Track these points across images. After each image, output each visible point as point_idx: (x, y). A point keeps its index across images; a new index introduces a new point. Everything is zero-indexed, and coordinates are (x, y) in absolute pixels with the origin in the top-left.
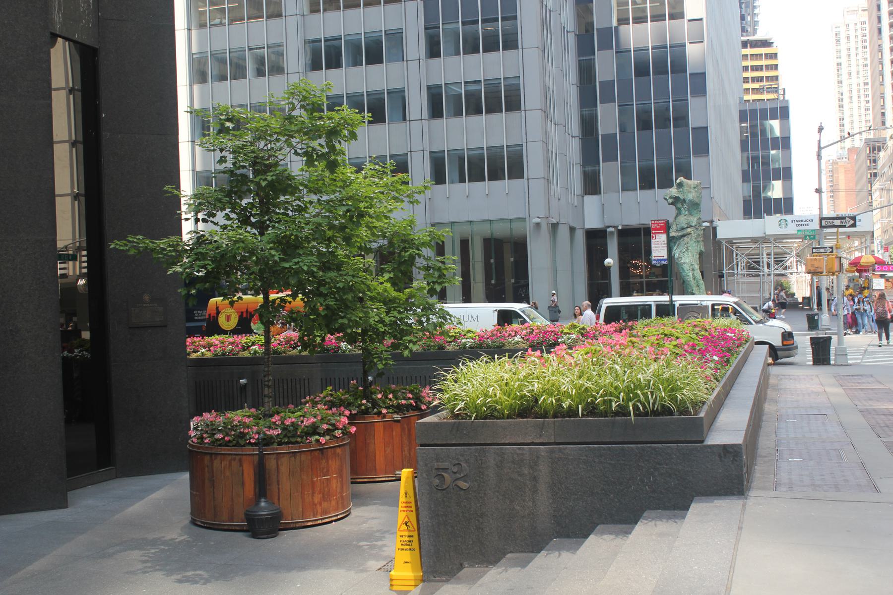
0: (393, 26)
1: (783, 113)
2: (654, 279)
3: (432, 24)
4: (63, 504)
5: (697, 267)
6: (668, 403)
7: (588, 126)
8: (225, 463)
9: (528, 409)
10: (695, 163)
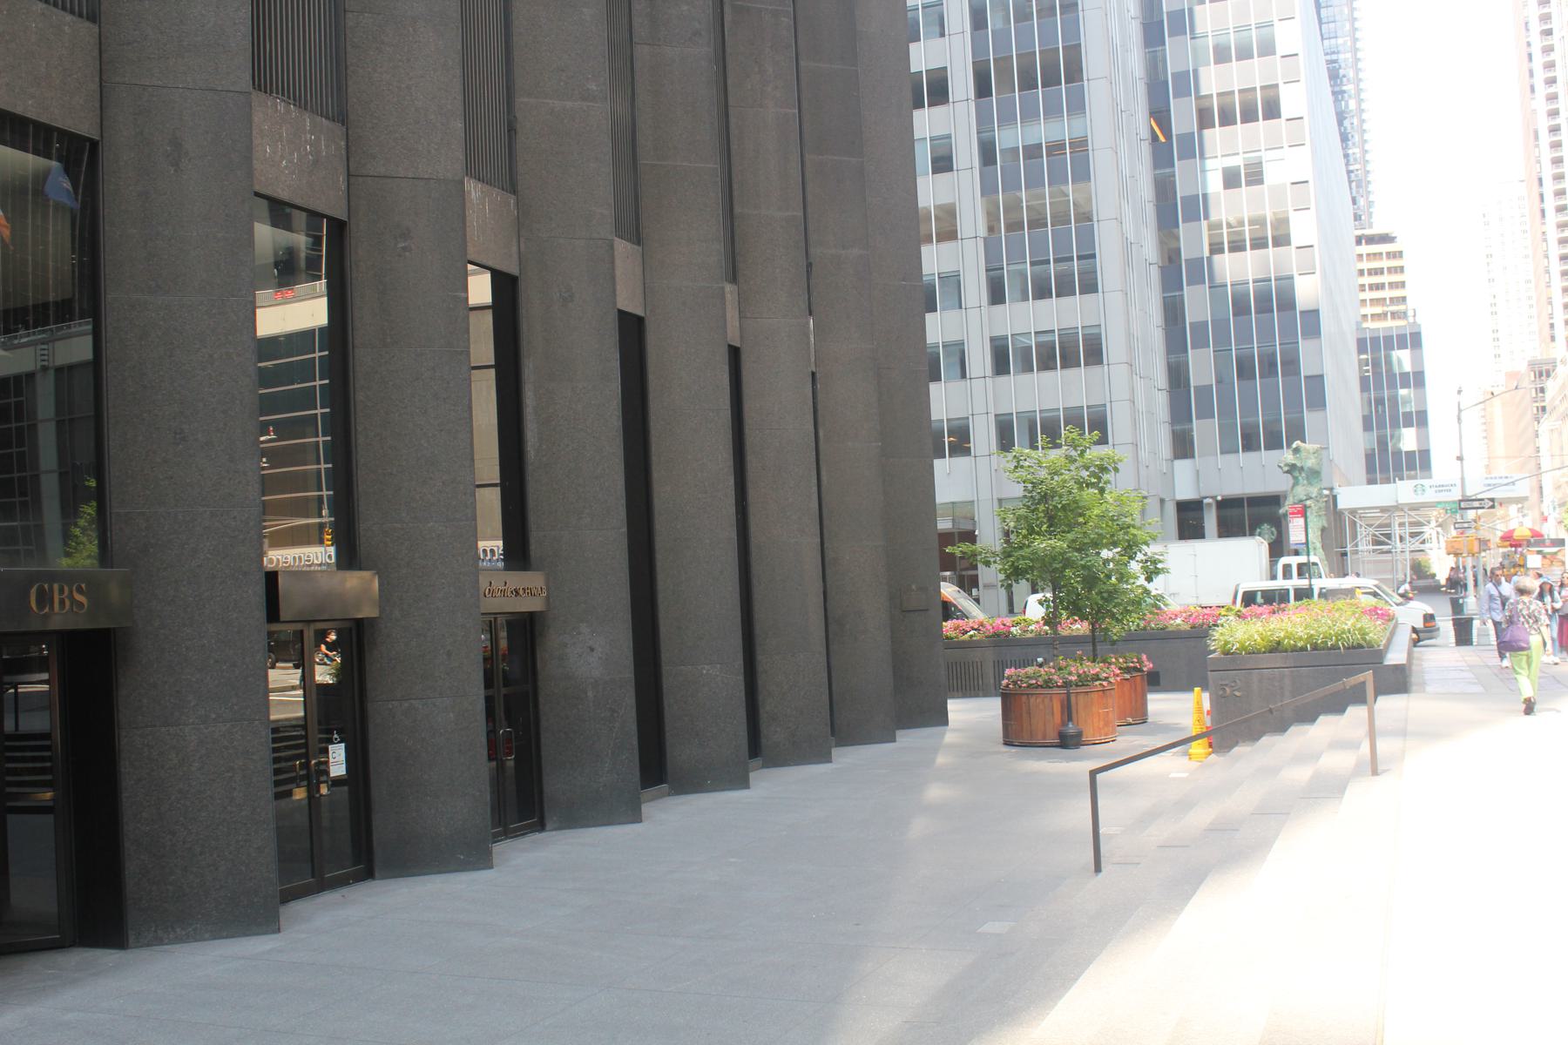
1: (1414, 340)
3: (996, 265)
4: (744, 783)
7: (1177, 377)
9: (1276, 648)
10: (1309, 418)
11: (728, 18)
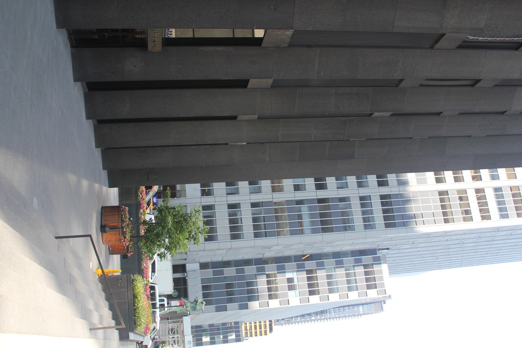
0: (263, 189)
1: (238, 339)
3: (264, 205)
4: (88, 118)
7: (227, 264)
9: (135, 297)
11: (343, 118)
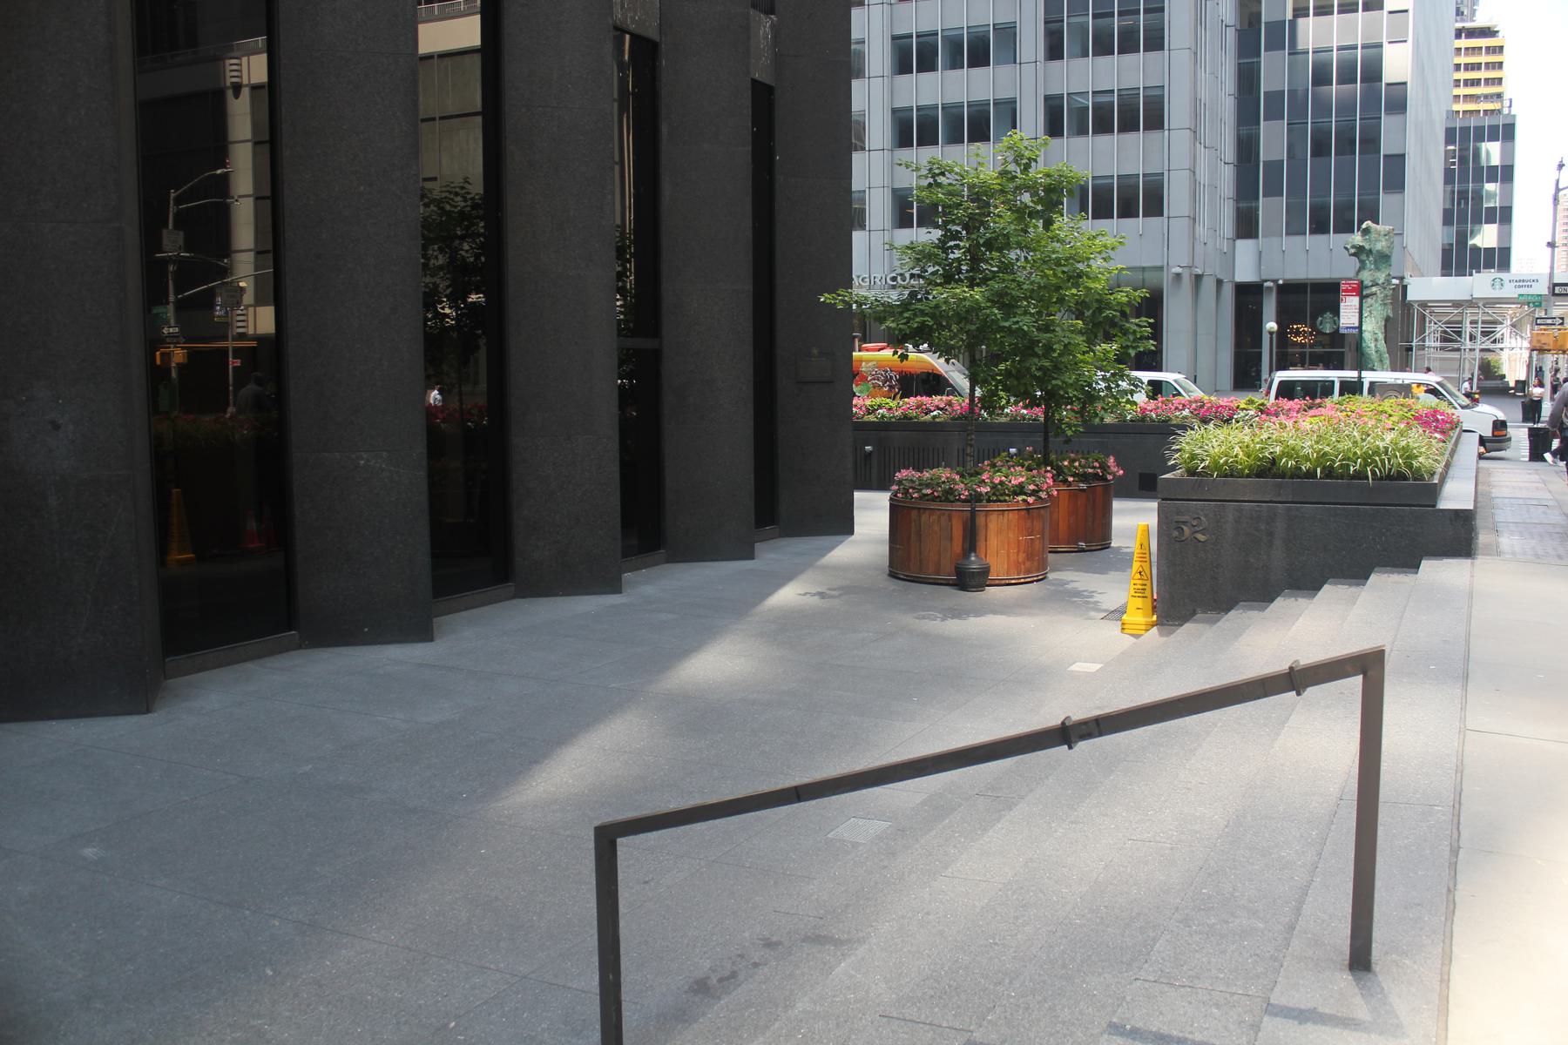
1: (1506, 132)
2: (1319, 350)
4: (424, 633)
5: (1381, 336)
6: (1404, 469)
7: (1247, 149)
8: (934, 518)
9: (1267, 469)
